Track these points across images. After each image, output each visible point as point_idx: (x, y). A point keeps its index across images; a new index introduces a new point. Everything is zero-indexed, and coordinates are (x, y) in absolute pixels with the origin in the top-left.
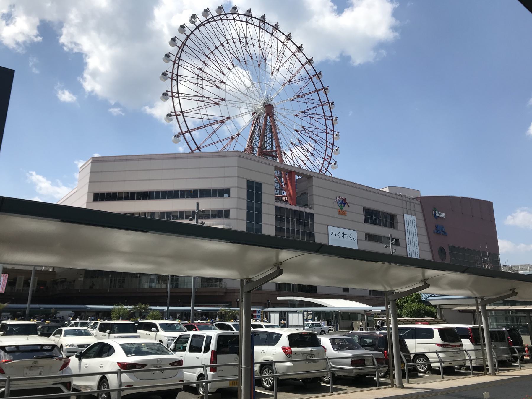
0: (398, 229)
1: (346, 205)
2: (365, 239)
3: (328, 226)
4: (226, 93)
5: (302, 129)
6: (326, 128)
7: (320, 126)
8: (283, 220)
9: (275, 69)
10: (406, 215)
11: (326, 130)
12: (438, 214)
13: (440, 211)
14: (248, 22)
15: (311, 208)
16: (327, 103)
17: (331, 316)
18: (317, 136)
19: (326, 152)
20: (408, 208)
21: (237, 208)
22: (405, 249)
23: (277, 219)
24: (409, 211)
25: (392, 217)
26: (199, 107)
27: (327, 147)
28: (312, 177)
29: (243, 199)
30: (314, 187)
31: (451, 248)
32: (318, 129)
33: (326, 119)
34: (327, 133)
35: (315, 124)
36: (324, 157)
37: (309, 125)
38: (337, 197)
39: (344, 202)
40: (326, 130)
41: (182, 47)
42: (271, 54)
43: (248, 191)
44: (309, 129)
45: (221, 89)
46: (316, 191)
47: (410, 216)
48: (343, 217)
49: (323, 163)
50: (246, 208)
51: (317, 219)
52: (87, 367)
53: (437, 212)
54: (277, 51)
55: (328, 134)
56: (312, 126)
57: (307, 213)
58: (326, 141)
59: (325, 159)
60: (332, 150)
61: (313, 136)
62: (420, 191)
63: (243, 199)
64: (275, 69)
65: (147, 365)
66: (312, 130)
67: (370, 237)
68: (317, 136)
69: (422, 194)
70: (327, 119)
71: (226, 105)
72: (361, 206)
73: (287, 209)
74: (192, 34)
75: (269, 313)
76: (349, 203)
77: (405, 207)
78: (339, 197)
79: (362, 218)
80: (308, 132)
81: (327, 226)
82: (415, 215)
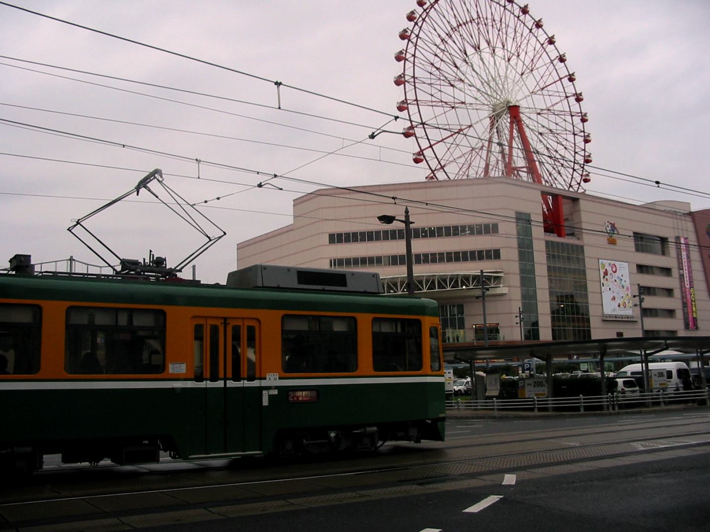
0: (670, 257)
2: (636, 272)
4: (453, 95)
6: (415, 84)
7: (427, 88)
9: (529, 69)
11: (414, 82)
15: (579, 239)
16: (581, 132)
19: (416, 48)
21: (511, 300)
23: (548, 258)
28: (578, 199)
30: (582, 212)
32: (428, 84)
33: (416, 100)
34: (414, 77)
37: (443, 88)
38: (606, 222)
40: (414, 82)
42: (551, 76)
43: (519, 251)
45: (456, 88)
46: (584, 217)
50: (518, 272)
51: (587, 251)
55: (412, 75)
56: (438, 87)
57: (577, 246)
58: (416, 64)
59: (417, 36)
60: (408, 51)
61: (437, 73)
62: (689, 203)
64: (529, 69)
66: (438, 82)
67: (642, 269)
69: (694, 209)
70: (415, 101)
75: (546, 334)
77: (680, 228)
78: (608, 222)
79: (631, 244)
80: (443, 78)
81: (597, 260)
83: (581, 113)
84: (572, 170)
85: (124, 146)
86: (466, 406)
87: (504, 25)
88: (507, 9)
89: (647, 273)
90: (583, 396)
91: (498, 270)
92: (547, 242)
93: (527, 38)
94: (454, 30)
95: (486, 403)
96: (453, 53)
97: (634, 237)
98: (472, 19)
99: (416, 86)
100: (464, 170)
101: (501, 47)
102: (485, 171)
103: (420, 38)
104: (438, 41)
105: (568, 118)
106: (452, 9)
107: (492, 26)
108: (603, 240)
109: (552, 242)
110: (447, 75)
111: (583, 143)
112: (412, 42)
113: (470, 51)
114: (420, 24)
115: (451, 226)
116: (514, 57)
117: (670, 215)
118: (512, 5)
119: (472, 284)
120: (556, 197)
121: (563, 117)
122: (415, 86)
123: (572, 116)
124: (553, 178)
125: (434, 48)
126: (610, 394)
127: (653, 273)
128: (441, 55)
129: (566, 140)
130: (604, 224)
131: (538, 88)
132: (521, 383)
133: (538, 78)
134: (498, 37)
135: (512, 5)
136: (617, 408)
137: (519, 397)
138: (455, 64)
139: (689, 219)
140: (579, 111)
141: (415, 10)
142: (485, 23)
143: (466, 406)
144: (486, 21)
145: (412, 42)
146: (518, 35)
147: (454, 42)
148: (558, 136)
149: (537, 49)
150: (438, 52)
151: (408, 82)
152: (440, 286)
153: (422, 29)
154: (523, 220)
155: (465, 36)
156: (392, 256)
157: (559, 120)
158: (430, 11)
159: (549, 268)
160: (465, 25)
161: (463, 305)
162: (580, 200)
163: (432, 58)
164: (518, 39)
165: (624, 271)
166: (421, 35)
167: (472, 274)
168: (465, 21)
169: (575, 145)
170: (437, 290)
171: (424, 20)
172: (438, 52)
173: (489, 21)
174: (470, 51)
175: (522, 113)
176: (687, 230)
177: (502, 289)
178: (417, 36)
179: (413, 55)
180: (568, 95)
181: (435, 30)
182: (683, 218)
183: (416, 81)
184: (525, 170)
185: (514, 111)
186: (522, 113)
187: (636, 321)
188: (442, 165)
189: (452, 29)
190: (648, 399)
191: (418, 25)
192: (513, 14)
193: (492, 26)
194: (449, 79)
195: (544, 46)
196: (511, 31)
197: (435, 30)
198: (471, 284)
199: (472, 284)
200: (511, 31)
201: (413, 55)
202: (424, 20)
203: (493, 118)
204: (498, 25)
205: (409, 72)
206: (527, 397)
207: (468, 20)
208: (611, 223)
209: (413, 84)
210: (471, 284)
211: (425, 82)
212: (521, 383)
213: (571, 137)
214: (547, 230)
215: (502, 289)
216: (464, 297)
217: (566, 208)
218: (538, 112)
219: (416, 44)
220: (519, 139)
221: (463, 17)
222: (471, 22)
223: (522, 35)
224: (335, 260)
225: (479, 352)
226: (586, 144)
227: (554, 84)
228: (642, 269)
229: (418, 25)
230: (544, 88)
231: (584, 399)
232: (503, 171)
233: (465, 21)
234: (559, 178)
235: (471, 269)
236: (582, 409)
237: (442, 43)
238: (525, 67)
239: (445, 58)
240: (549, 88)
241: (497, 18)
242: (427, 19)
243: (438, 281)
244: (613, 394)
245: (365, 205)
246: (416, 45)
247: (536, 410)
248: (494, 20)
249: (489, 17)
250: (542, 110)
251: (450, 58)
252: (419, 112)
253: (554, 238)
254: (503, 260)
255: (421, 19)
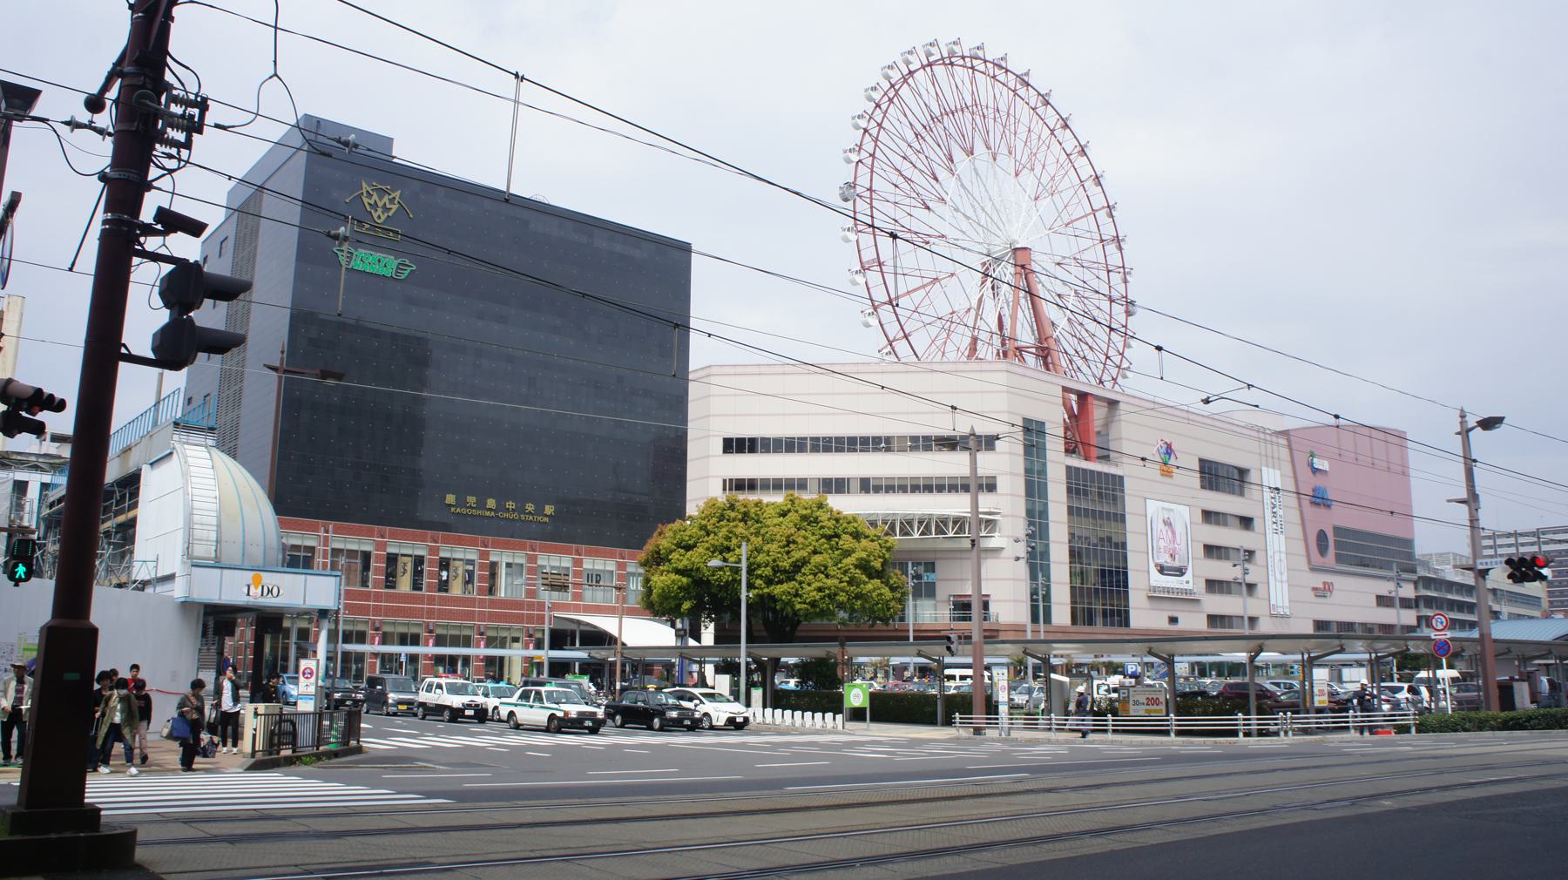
1: (1172, 456)
3: (1146, 499)
5: (930, 204)
7: (889, 209)
8: (1078, 492)
10: (1264, 469)
11: (871, 199)
12: (1318, 463)
13: (1321, 457)
14: (1017, 92)
17: (1005, 222)
18: (896, 186)
19: (876, 145)
20: (1269, 454)
22: (1263, 537)
24: (1270, 460)
25: (1243, 472)
26: (10, 259)
27: (873, 155)
28: (1118, 402)
29: (1019, 496)
31: (1338, 530)
34: (870, 189)
35: (899, 215)
36: (882, 130)
37: (914, 211)
39: (1169, 450)
40: (871, 199)
41: (899, 85)
42: (1066, 176)
44: (914, 203)
47: (1271, 470)
48: (1168, 480)
49: (883, 118)
52: (890, 547)
53: (1315, 460)
54: (1044, 166)
59: (880, 125)
61: (905, 186)
63: (1019, 496)
64: (1047, 191)
65: (1003, 548)
67: (1209, 516)
68: (896, 186)
70: (1111, 271)
71: (852, 214)
72: (1195, 455)
73: (1092, 472)
74: (922, 70)
76: (1178, 451)
77: (1263, 453)
79: (1195, 480)
82: (1280, 469)
83: (1123, 267)
84: (1105, 357)
85: (710, 335)
86: (1025, 724)
87: (1012, 119)
88: (1018, 95)
89: (1218, 523)
90: (1176, 716)
91: (992, 510)
92: (1069, 468)
93: (1047, 142)
94: (935, 120)
95: (1083, 720)
96: (933, 156)
97: (1202, 471)
98: (964, 106)
99: (874, 204)
100: (938, 343)
101: (1007, 153)
102: (970, 349)
103: (884, 129)
104: (910, 136)
105: (1104, 275)
106: (933, 84)
107: (995, 119)
108: (1153, 471)
109: (1077, 469)
110: (921, 191)
111: (1124, 315)
112: (870, 135)
113: (958, 154)
114: (884, 107)
115: (920, 435)
116: (1025, 171)
117: (1254, 434)
118: (1027, 89)
119: (953, 529)
120: (1083, 397)
121: (1095, 272)
122: (871, 204)
123: (1109, 271)
124: (1075, 368)
125: (904, 146)
126: (1281, 714)
127: (1225, 524)
128: (913, 158)
129: (1098, 308)
130: (1155, 443)
131: (1059, 222)
132: (1124, 693)
133: (1061, 207)
134: (1002, 138)
135: (1027, 89)
136: (1290, 733)
137: (1120, 714)
138: (933, 174)
139: (1283, 441)
140: (1121, 265)
141: (878, 84)
142: (983, 114)
143: (1025, 724)
144: (985, 111)
145: (870, 135)
146: (1034, 136)
147: (939, 146)
148: (1086, 301)
149: (1061, 161)
150: (909, 152)
151: (860, 197)
152: (940, 531)
153: (887, 115)
154: (1033, 432)
155: (952, 130)
156: (823, 479)
157: (1088, 276)
158: (901, 86)
159: (1070, 510)
160: (953, 115)
161: (934, 563)
162: (1121, 404)
163: (898, 162)
164: (1034, 143)
165: (1184, 515)
166: (886, 124)
167: (953, 514)
168: (953, 109)
169: (1111, 317)
170: (898, 537)
171: (891, 100)
172: (909, 152)
173: (991, 111)
174: (958, 154)
175: (1034, 261)
176: (1279, 459)
177: (994, 542)
178: (880, 125)
179: (871, 155)
180: (1104, 238)
181: (905, 115)
182: (1274, 439)
183: (874, 196)
184: (1033, 350)
185: (1021, 258)
186: (1034, 261)
187: (1198, 600)
188: (907, 332)
189: (932, 119)
190: (1073, 720)
191: (880, 108)
192: (1028, 104)
193: (995, 119)
194: (924, 197)
195: (1071, 157)
196: (1022, 129)
197: (905, 115)
198: (950, 530)
199: (953, 529)
200: (1022, 129)
201: (871, 155)
202: (891, 100)
203: (988, 264)
204: (1004, 118)
205: (864, 181)
206: (1132, 713)
207: (959, 107)
208: (1166, 443)
209: (868, 201)
210: (950, 530)
211: (888, 198)
212: (1124, 693)
213: (1105, 304)
214: (1070, 451)
215: (994, 542)
216: (935, 551)
217: (1098, 413)
218: (1058, 259)
219: (877, 139)
220: (1027, 301)
221: (952, 101)
222: (962, 110)
223: (1040, 137)
224: (731, 480)
225: (1055, 645)
226: (1129, 318)
227: (1085, 219)
228: (1209, 516)
229: (880, 108)
230: (1069, 223)
231: (1113, 720)
232: (998, 350)
233: (953, 109)
234: (1084, 368)
235: (954, 505)
236: (1241, 734)
237: (916, 139)
238: (1041, 188)
239: (919, 165)
240: (1076, 224)
241: (1003, 108)
242: (895, 100)
243: (901, 523)
244: (1285, 714)
245: (784, 394)
246: (876, 140)
247: (1173, 734)
248: (998, 110)
249: (991, 104)
250: (1064, 258)
251: (927, 165)
252: (876, 245)
253: (1077, 462)
254: (1002, 495)
255: (886, 98)
